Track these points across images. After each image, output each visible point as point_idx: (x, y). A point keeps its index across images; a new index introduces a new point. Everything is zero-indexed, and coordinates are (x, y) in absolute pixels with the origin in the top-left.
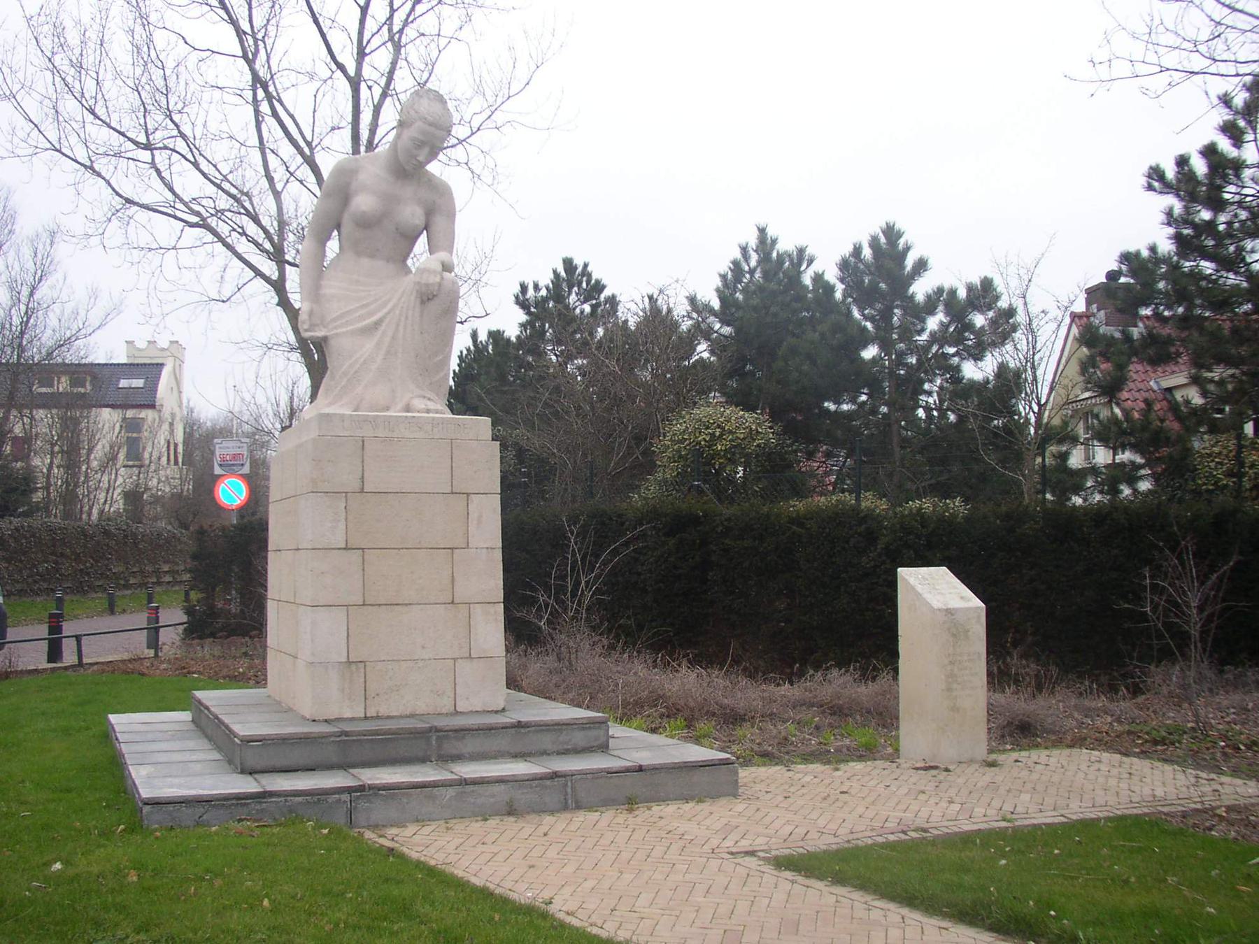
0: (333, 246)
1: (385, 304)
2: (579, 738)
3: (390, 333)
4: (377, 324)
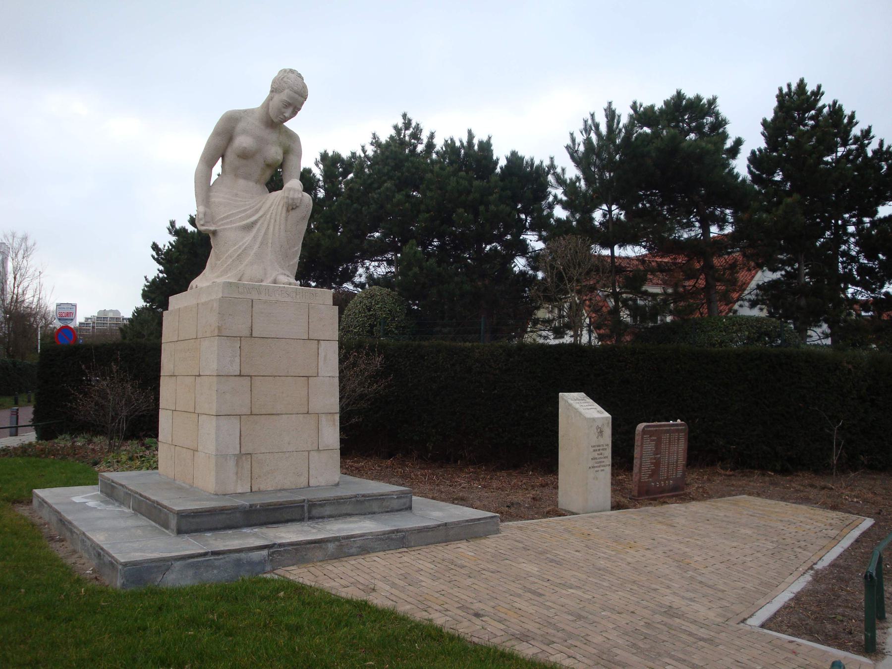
0: (217, 169)
1: (257, 211)
2: (395, 504)
3: (263, 231)
4: (254, 223)
